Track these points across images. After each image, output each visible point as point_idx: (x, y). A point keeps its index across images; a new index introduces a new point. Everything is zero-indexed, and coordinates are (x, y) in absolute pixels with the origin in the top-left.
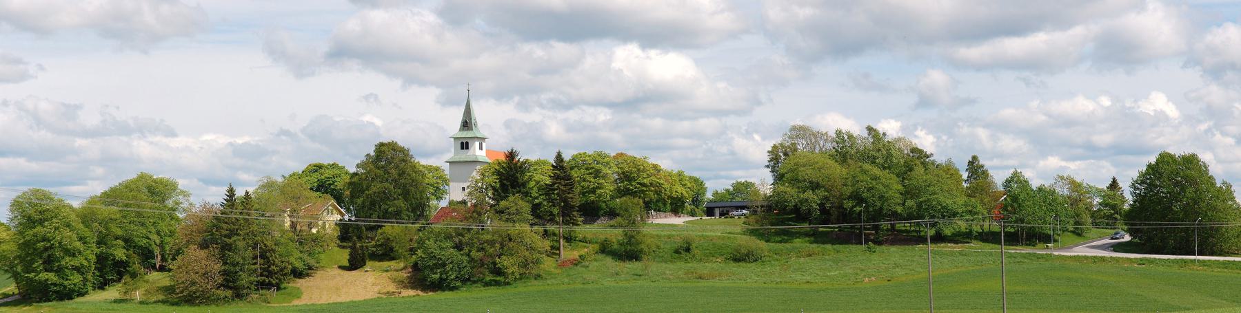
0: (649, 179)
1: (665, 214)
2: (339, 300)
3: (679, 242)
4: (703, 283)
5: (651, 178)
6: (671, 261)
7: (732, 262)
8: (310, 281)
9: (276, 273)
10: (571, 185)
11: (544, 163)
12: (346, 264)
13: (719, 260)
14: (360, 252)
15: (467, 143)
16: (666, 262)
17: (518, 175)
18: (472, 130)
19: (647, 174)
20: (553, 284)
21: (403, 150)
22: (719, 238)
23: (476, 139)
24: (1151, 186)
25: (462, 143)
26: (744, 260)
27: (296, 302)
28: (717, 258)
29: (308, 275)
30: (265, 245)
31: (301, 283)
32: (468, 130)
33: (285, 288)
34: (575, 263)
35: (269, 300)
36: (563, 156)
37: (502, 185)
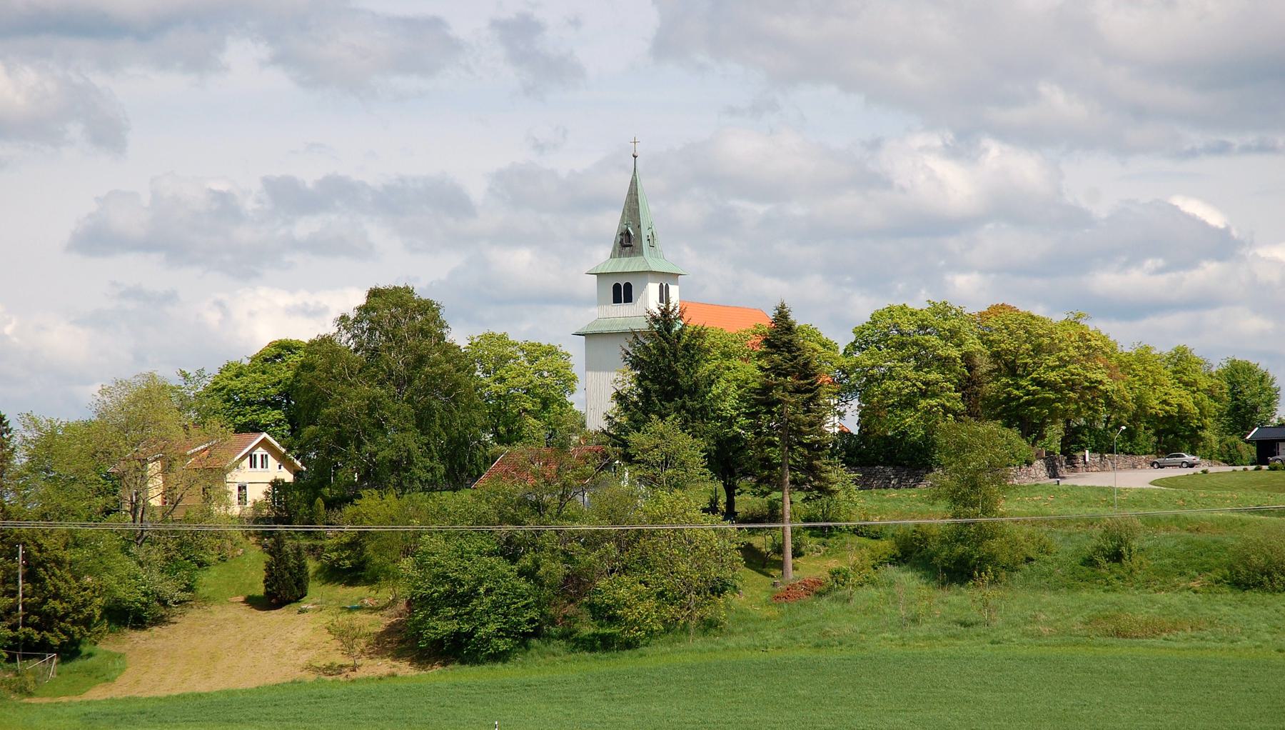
0: (1062, 371)
1: (1130, 459)
2: (202, 688)
3: (1091, 541)
4: (1121, 648)
5: (1070, 367)
6: (1069, 587)
7: (1226, 589)
8: (159, 637)
9: (62, 619)
10: (811, 391)
11: (303, 342)
12: (260, 590)
13: (1196, 585)
14: (292, 562)
15: (628, 287)
16: (1055, 590)
17: (679, 367)
18: (641, 253)
19: (1060, 359)
20: (739, 648)
21: (426, 307)
22: (1229, 525)
23: (649, 275)
24: (430, 656)
25: (617, 288)
26: (1259, 585)
27: (98, 693)
28: (1193, 579)
29: (159, 621)
30: (40, 548)
31: (137, 638)
32: (631, 254)
33: (90, 655)
34: (817, 590)
35: (31, 687)
36: (792, 317)
37: (646, 395)
